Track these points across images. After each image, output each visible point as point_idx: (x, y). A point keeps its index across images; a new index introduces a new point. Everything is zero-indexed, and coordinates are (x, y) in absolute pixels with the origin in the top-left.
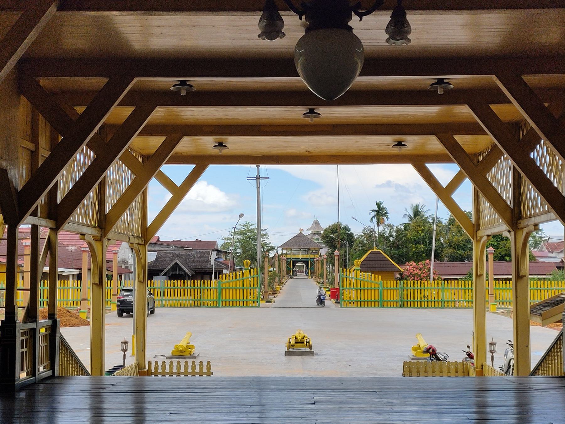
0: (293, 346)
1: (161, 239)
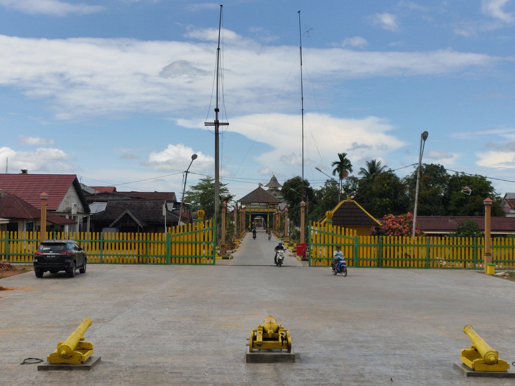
0: (259, 345)
1: (118, 190)
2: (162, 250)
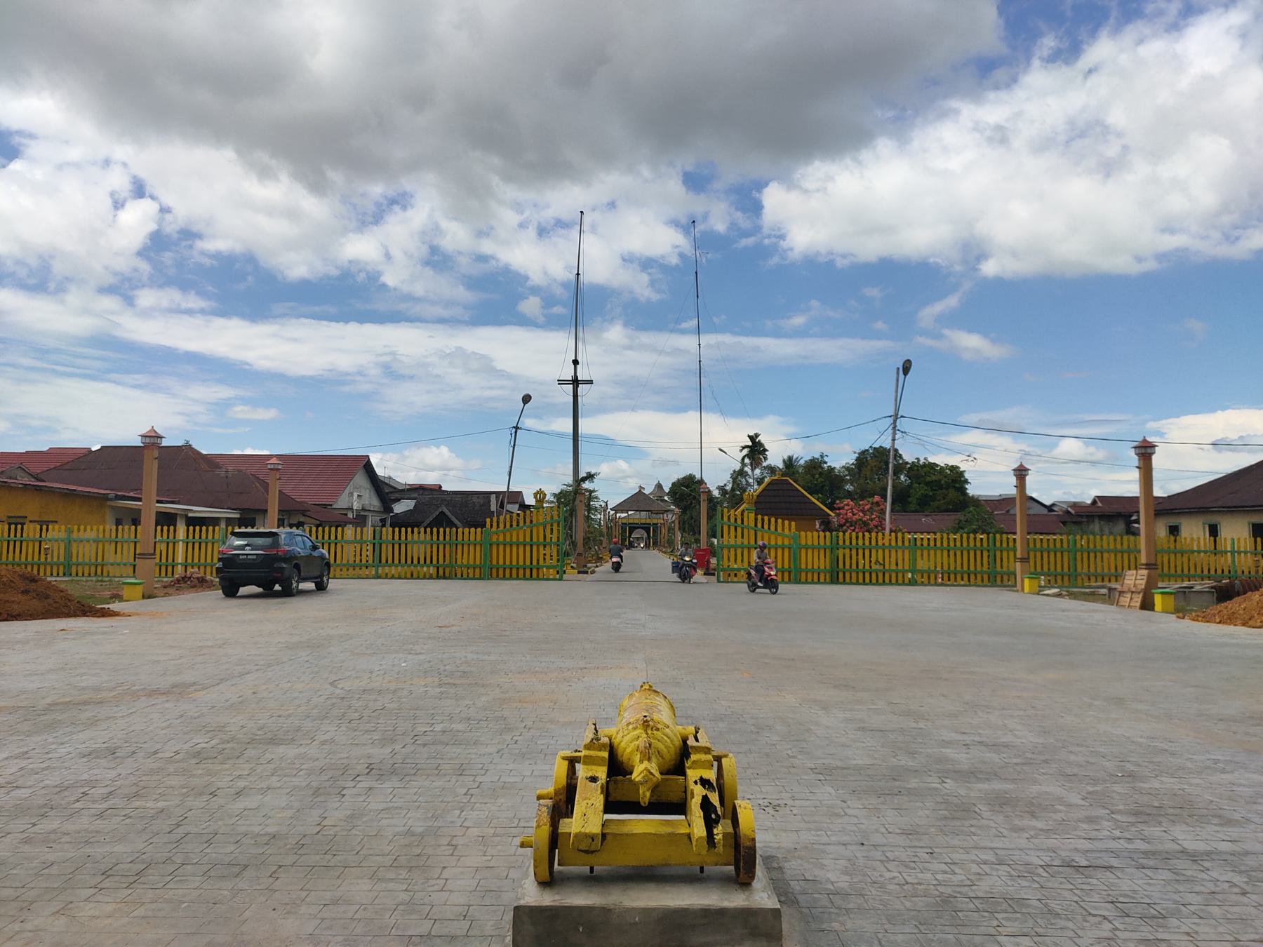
2: (471, 556)
